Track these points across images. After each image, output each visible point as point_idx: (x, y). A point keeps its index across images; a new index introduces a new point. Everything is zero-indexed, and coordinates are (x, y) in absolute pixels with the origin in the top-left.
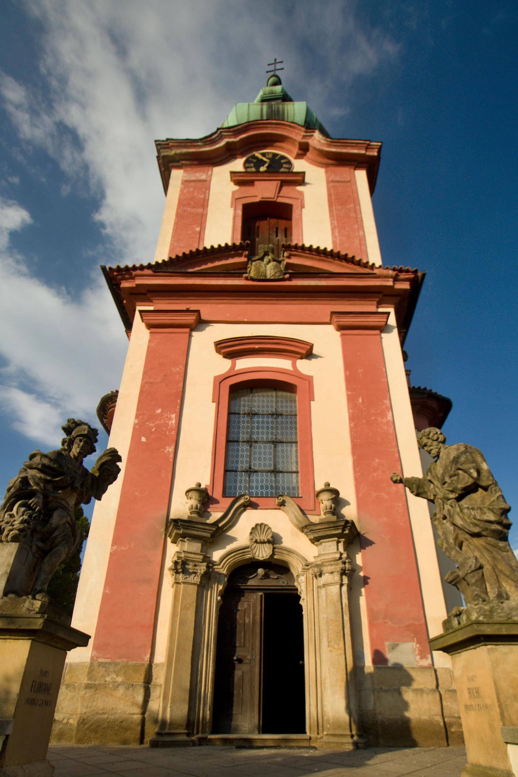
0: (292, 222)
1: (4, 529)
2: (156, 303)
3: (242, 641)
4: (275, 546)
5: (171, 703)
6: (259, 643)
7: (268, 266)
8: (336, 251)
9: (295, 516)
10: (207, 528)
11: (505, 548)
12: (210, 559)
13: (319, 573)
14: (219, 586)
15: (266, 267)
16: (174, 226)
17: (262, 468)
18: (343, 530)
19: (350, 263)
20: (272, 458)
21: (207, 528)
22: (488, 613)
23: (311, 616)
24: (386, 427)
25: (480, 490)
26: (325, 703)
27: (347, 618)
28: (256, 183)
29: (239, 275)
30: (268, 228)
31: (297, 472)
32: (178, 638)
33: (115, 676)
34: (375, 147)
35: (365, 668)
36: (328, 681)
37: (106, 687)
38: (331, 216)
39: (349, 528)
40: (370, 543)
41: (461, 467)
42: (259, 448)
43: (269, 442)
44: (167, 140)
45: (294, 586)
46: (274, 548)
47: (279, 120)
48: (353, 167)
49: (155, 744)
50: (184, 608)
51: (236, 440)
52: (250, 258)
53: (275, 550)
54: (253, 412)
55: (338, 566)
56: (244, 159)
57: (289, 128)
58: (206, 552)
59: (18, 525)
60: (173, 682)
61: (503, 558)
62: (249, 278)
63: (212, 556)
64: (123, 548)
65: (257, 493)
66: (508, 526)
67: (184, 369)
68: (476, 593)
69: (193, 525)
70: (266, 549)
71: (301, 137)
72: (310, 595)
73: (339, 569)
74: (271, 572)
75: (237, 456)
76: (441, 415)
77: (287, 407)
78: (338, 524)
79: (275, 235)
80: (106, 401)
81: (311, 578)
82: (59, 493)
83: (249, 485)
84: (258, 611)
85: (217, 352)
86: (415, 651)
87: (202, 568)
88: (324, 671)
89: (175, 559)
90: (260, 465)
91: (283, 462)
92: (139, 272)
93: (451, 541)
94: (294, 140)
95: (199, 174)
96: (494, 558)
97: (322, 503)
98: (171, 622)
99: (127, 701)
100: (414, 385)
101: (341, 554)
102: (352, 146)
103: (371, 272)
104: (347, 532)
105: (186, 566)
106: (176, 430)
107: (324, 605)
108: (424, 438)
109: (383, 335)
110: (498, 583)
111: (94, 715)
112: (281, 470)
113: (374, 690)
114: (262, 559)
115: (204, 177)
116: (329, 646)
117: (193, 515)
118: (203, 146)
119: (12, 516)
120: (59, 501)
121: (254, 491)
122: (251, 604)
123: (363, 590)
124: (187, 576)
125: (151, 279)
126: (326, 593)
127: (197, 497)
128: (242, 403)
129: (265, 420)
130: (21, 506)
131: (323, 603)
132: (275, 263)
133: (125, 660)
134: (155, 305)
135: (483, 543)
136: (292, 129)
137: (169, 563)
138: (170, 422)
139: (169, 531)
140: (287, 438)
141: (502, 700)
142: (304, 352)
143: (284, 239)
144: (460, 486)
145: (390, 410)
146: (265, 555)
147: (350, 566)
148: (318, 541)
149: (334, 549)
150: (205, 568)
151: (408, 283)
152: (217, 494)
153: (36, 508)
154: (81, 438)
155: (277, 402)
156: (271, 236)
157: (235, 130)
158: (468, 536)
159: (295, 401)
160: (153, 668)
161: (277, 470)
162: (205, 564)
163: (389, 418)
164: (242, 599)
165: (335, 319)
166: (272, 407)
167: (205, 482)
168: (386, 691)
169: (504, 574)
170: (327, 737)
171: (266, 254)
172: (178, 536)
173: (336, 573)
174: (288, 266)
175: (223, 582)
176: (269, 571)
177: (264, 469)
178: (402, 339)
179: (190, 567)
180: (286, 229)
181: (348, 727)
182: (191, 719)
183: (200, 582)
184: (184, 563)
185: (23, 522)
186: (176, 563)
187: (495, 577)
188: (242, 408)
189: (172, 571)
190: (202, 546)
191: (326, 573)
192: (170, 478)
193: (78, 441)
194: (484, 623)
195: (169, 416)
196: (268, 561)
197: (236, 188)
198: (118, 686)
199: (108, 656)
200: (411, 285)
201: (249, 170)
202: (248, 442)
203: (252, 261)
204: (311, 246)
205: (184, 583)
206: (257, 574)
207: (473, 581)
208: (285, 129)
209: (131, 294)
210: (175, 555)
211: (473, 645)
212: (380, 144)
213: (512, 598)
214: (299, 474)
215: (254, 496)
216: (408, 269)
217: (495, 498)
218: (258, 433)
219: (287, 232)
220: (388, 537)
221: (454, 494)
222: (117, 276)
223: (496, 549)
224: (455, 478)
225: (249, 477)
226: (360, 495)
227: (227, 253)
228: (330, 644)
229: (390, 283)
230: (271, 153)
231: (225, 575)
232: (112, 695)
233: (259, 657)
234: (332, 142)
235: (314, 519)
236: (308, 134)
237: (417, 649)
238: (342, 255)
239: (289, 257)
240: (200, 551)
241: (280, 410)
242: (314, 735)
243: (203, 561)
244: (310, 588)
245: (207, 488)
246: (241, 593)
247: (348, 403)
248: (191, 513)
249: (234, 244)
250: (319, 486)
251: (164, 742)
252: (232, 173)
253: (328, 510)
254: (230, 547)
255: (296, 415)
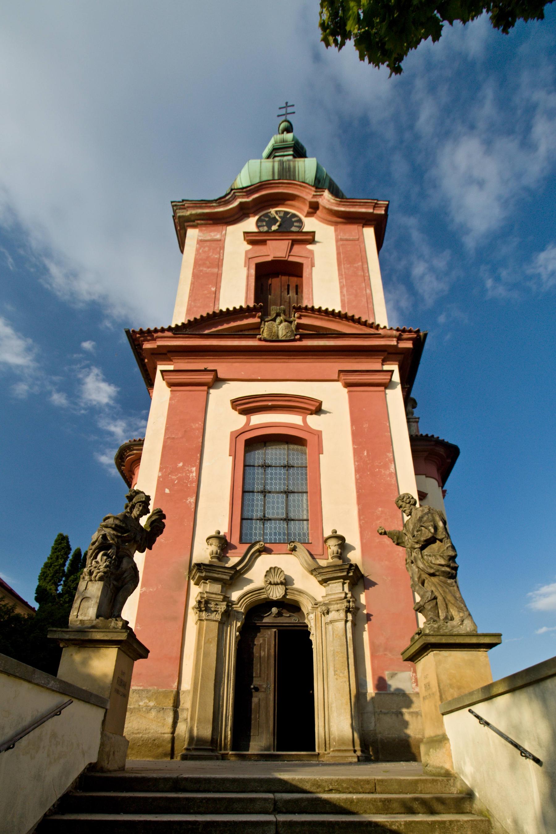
0: (302, 279)
1: (93, 572)
2: (176, 363)
3: (258, 672)
4: (287, 587)
5: (197, 723)
6: (273, 674)
7: (280, 327)
8: (343, 312)
9: (306, 561)
10: (226, 571)
11: (452, 584)
12: (230, 599)
13: (326, 611)
14: (238, 622)
15: (278, 327)
16: (191, 286)
17: (275, 516)
18: (348, 573)
19: (357, 324)
20: (285, 507)
21: (226, 571)
22: (436, 630)
23: (319, 649)
24: (389, 478)
25: (438, 541)
26: (331, 724)
27: (351, 650)
28: (268, 242)
29: (253, 336)
30: (280, 285)
31: (307, 520)
32: (202, 667)
33: (147, 701)
34: (382, 205)
35: (368, 694)
36: (334, 705)
37: (140, 711)
38: (340, 274)
39: (353, 570)
40: (373, 584)
41: (423, 525)
42: (271, 498)
43: (282, 492)
44: (183, 201)
45: (305, 623)
46: (286, 589)
47: (291, 180)
48: (362, 225)
49: (185, 758)
50: (207, 642)
51: (251, 490)
52: (262, 319)
53: (288, 591)
54: (266, 465)
55: (343, 605)
56: (257, 217)
57: (300, 188)
58: (226, 592)
59: (103, 569)
60: (199, 706)
61: (450, 591)
62: (262, 339)
63: (231, 596)
64: (151, 590)
65: (271, 539)
66: (456, 569)
67: (202, 425)
68: (431, 616)
69: (214, 569)
70: (279, 590)
71: (311, 196)
72: (319, 631)
73: (344, 607)
74: (284, 611)
75: (253, 506)
76: (449, 461)
77: (298, 459)
78: (343, 568)
79: (286, 293)
80: (124, 450)
81: (320, 615)
82: (126, 545)
83: (264, 531)
84: (273, 646)
85: (233, 409)
86: (411, 680)
87: (223, 607)
88: (331, 697)
89: (199, 598)
90: (273, 513)
91: (294, 511)
92: (160, 334)
93: (416, 579)
94: (305, 199)
95: (214, 233)
96: (444, 591)
97: (330, 548)
98: (196, 654)
99: (158, 722)
100: (422, 433)
101: (346, 594)
102: (360, 205)
103: (376, 332)
104: (351, 574)
105: (209, 605)
106: (197, 483)
107: (331, 639)
108: (400, 501)
109: (388, 391)
110: (446, 609)
111: (129, 734)
112: (292, 518)
113: (375, 713)
114: (276, 599)
115: (218, 237)
116: (335, 675)
117: (214, 560)
118: (217, 206)
119: (97, 562)
120: (125, 551)
121: (268, 537)
122: (266, 639)
123: (366, 626)
124: (210, 614)
125: (171, 340)
126: (333, 628)
127: (217, 544)
128: (257, 456)
129: (278, 471)
130: (103, 555)
131: (330, 638)
132: (286, 323)
133: (156, 688)
134: (175, 364)
135: (438, 581)
136: (302, 188)
137: (193, 602)
138: (191, 475)
139: (193, 574)
140: (298, 488)
141: (441, 687)
142: (313, 408)
143: (295, 296)
144: (423, 539)
145: (393, 462)
146: (278, 595)
147: (354, 604)
148: (326, 582)
149: (340, 590)
150: (225, 607)
151: (411, 342)
152: (235, 540)
153: (113, 556)
154: (140, 504)
155: (288, 455)
156: (283, 294)
157: (248, 190)
158: (427, 576)
159: (306, 454)
160: (181, 694)
161: (289, 518)
162: (225, 603)
163: (391, 469)
164: (258, 634)
165: (342, 377)
166: (284, 459)
167: (224, 530)
168: (385, 714)
169: (451, 603)
170: (333, 753)
171: (278, 315)
172: (200, 578)
173: (341, 611)
174: (299, 326)
175: (241, 620)
176: (282, 610)
177: (277, 517)
178: (405, 394)
179: (212, 605)
180: (297, 287)
181: (351, 743)
182: (215, 737)
183: (221, 619)
184: (207, 602)
185: (106, 567)
186: (199, 602)
187: (445, 605)
188: (256, 461)
189: (195, 609)
190: (222, 587)
191: (333, 611)
192: (192, 526)
193: (138, 506)
194: (430, 635)
195: (189, 470)
196: (281, 600)
197: (250, 247)
198: (151, 710)
199: (141, 684)
200: (413, 344)
201: (262, 229)
202: (262, 492)
203: (265, 322)
204: (320, 308)
205: (207, 620)
206: (271, 613)
207: (429, 608)
208: (296, 188)
209: (153, 354)
210: (198, 595)
211: (425, 652)
212: (387, 203)
213: (455, 620)
214: (309, 521)
215: (268, 542)
216: (411, 329)
217: (445, 548)
218: (271, 484)
219: (298, 289)
220: (389, 578)
221: (418, 545)
222: (139, 337)
223: (446, 585)
224: (419, 533)
225: (264, 525)
226: (364, 541)
227: (241, 315)
228: (336, 673)
229: (394, 342)
230: (282, 211)
231: (243, 613)
232: (145, 717)
233: (273, 685)
234: (341, 202)
235: (323, 563)
236: (318, 193)
237: (413, 677)
238: (349, 316)
239: (299, 318)
240: (220, 591)
241: (291, 463)
242: (322, 751)
243: (223, 601)
244: (319, 625)
245: (226, 535)
246: (257, 629)
247: (354, 456)
248: (212, 558)
249: (248, 306)
250: (327, 533)
251: (193, 755)
252: (246, 233)
253: (335, 555)
254: (247, 588)
255: (307, 467)
